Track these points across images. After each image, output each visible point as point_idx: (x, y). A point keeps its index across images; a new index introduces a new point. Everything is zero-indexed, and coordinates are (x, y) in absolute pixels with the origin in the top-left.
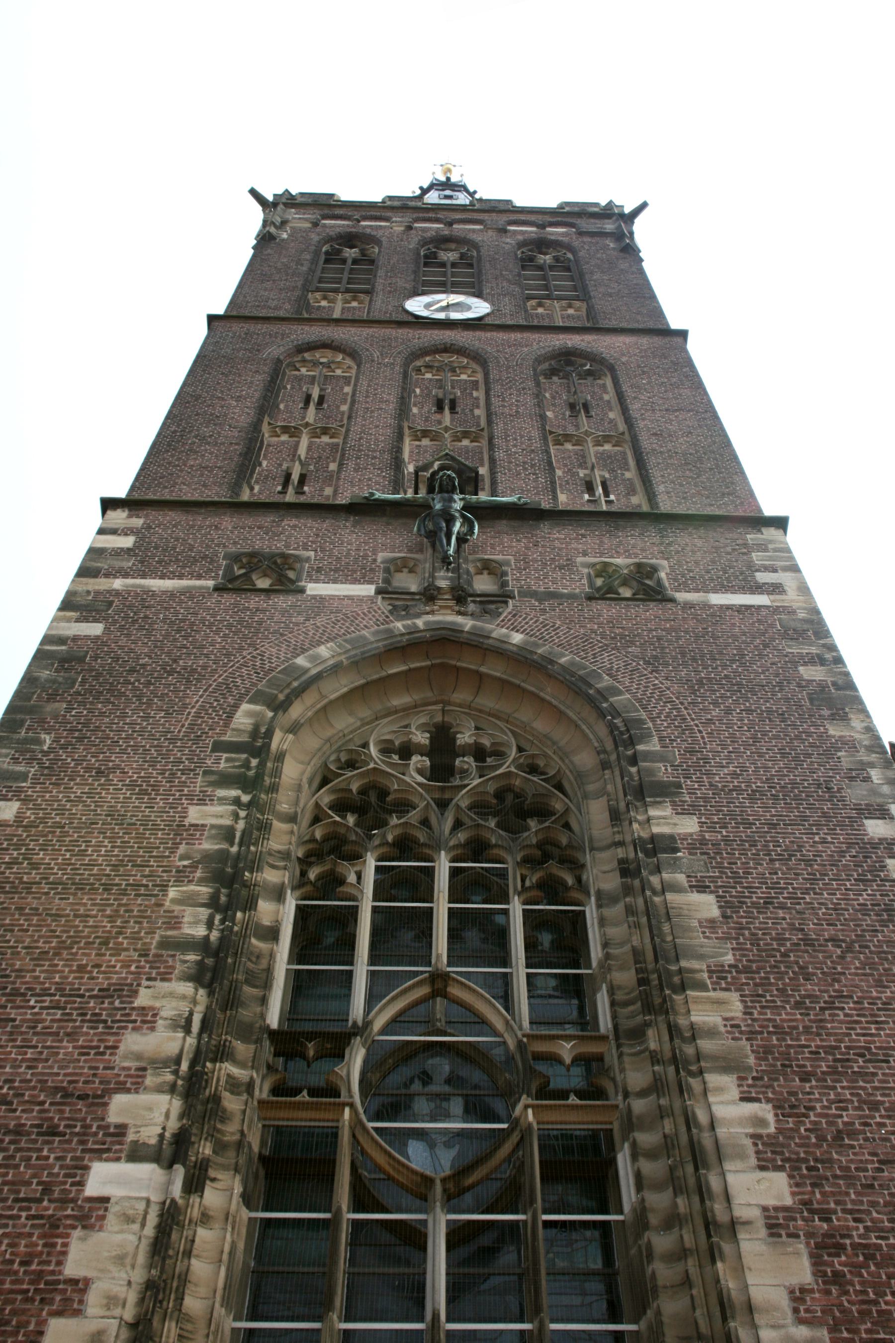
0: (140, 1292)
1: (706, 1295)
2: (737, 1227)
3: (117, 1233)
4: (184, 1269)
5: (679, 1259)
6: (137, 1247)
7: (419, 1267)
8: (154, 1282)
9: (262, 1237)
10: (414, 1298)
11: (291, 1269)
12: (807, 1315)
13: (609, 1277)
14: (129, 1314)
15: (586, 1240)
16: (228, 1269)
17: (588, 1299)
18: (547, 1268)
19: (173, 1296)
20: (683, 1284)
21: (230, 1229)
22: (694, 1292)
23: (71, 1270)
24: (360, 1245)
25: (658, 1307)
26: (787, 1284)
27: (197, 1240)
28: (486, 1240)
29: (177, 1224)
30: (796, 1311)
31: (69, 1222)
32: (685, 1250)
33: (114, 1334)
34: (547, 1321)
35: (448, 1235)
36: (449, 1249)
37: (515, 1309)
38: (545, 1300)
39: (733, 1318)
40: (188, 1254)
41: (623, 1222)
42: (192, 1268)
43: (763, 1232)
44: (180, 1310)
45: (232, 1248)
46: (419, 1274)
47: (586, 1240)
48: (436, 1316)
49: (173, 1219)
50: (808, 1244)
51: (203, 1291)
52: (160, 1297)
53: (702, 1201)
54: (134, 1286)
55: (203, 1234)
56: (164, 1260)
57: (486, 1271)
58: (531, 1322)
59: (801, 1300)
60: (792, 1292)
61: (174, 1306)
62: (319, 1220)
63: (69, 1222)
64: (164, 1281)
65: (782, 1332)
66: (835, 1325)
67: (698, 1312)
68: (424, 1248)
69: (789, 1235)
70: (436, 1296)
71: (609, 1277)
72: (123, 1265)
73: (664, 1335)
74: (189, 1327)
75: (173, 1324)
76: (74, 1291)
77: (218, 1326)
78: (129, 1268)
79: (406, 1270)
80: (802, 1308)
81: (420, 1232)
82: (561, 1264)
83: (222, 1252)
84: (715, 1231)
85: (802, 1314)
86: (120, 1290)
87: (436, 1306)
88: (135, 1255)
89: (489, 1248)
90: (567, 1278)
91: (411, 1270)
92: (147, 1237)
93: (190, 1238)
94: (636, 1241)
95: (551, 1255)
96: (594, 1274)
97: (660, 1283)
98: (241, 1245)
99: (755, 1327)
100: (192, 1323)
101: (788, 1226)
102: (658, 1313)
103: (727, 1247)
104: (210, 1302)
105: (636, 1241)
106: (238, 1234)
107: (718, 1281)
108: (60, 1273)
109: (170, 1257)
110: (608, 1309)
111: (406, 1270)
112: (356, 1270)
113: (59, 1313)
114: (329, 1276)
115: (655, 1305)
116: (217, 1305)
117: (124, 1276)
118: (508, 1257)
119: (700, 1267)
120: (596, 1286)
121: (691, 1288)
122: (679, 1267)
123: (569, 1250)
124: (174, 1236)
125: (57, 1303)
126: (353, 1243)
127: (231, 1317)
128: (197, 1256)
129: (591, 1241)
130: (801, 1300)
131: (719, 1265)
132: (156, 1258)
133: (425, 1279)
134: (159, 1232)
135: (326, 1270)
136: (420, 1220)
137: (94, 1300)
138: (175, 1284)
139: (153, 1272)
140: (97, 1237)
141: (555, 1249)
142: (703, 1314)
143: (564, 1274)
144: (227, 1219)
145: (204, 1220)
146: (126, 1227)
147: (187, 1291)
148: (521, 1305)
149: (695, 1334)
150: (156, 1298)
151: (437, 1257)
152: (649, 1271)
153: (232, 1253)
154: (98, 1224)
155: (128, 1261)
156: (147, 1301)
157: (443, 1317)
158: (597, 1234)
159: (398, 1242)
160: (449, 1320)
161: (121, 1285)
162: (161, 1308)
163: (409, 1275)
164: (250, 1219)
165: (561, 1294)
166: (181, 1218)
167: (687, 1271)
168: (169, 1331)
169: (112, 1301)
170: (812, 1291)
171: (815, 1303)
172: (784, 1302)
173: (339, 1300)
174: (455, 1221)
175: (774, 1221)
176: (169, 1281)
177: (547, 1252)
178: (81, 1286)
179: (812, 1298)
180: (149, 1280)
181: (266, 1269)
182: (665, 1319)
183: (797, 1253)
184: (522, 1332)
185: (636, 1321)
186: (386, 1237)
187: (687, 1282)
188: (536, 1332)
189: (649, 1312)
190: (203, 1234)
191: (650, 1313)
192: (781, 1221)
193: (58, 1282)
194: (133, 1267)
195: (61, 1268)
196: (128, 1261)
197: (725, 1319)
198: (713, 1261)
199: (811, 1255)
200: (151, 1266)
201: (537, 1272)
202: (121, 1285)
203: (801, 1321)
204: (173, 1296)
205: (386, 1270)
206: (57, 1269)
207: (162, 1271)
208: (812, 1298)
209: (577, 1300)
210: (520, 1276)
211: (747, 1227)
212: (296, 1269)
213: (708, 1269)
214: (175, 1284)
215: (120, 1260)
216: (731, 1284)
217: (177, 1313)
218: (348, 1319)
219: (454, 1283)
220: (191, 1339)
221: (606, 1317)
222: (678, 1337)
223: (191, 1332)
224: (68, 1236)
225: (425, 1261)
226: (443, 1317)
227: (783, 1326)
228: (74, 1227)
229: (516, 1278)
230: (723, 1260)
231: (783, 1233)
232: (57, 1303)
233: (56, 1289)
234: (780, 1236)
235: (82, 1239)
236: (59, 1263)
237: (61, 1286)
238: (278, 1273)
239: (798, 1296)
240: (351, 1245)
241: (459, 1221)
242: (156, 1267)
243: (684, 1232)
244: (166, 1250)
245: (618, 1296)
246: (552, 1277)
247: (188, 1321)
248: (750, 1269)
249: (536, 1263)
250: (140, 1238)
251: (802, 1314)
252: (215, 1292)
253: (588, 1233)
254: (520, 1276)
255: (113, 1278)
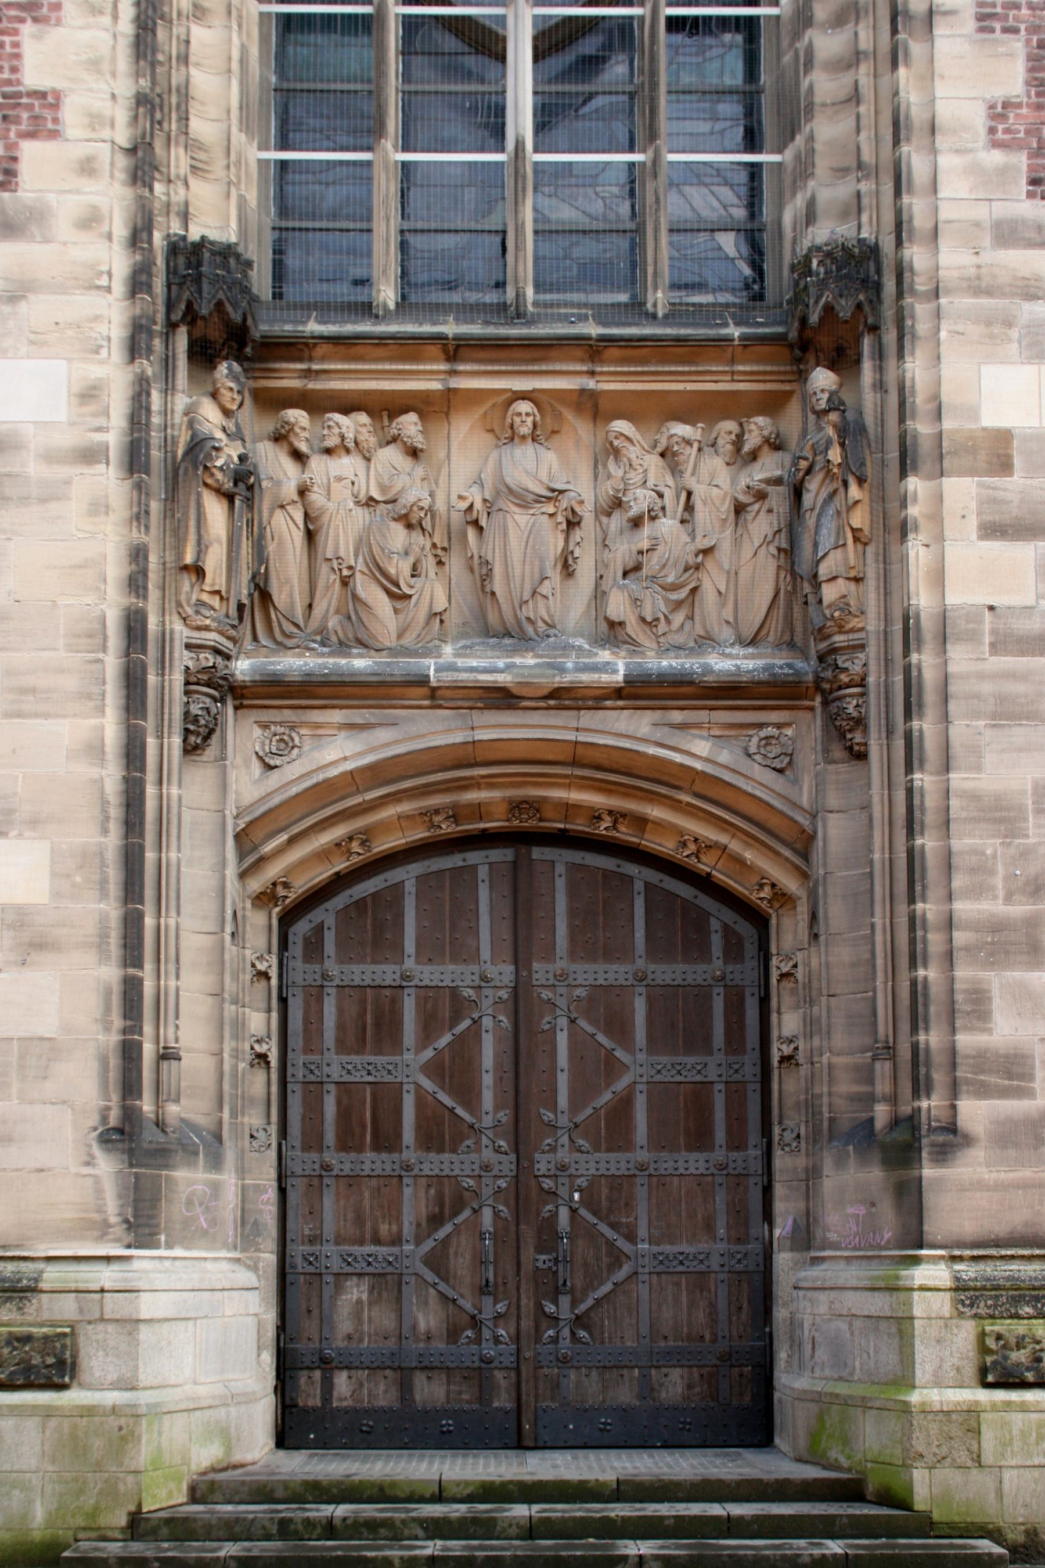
0: (131, 109)
1: (876, 112)
2: (936, 19)
3: (81, 28)
4: (183, 79)
5: (849, 67)
6: (114, 48)
7: (496, 83)
8: (146, 95)
9: (282, 44)
10: (492, 125)
11: (325, 86)
12: (1006, 137)
13: (750, 100)
14: (123, 137)
15: (723, 46)
16: (241, 83)
17: (719, 126)
18: (669, 85)
19: (174, 116)
20: (849, 100)
21: (235, 27)
22: (862, 109)
23: (32, 78)
24: (416, 53)
25: (812, 131)
26: (988, 96)
27: (193, 40)
28: (589, 46)
29: (162, 18)
30: (992, 131)
31: (13, 13)
32: (858, 53)
33: (108, 161)
34: (664, 151)
35: (535, 39)
36: (537, 58)
37: (623, 136)
38: (664, 125)
39: (921, 768)
40: (184, 59)
41: (778, 18)
42: (192, 80)
43: (971, 25)
44: (187, 134)
45: (242, 53)
46: (497, 93)
47: (723, 46)
48: (519, 145)
49: (155, 9)
50: (1028, 42)
51: (213, 112)
52: (158, 116)
53: (898, 193)
54: (119, 100)
55: (199, 33)
56: (153, 64)
57: (587, 88)
58: (644, 151)
59: (1002, 117)
60: (992, 107)
61: (179, 129)
62: (356, 16)
63: (13, 13)
64: (159, 96)
65: (969, 157)
66: (1039, 148)
67: (863, 135)
68: (502, 58)
69: (1005, 30)
70: (520, 119)
71: (750, 100)
72: (99, 72)
73: (813, 166)
74: (202, 156)
75: (181, 151)
76: (43, 106)
77: (239, 155)
78: (108, 77)
79: (480, 88)
80: (1000, 127)
81: (497, 35)
82: (687, 79)
83: (230, 58)
84: (904, 25)
85: (1000, 135)
86: (103, 105)
87: (521, 131)
88: (113, 59)
89: (591, 57)
90: (694, 97)
91: (485, 88)
92: (124, 35)
93: (183, 37)
94: (791, 44)
95: (675, 66)
96: (731, 92)
97: (818, 99)
98: (254, 51)
99: (934, 151)
100: (206, 151)
101: (1006, 17)
102: (811, 138)
103: (916, 48)
104: (225, 126)
105: (791, 44)
106: (248, 35)
107: (896, 93)
108: (19, 82)
109: (161, 63)
110: (745, 138)
111: (480, 88)
112: (412, 88)
113: (31, 135)
114: (376, 95)
115: (808, 128)
116: (234, 130)
117: (105, 87)
118: (617, 69)
119: (875, 76)
120: (731, 108)
121: (858, 103)
122: (846, 79)
123: (700, 59)
124: (161, 34)
125: (25, 122)
126: (407, 51)
127: (255, 145)
128: (197, 65)
129: (731, 47)
130: (1002, 117)
131: (902, 71)
132: (142, 63)
133: (505, 99)
134: (139, 27)
135: (372, 87)
136: (497, 16)
137: (71, 115)
138: (174, 100)
139: (142, 82)
140: (55, 34)
141: (681, 59)
142: (869, 138)
143: (690, 92)
144: (229, 13)
145: (199, 15)
146: (91, 20)
147: (191, 110)
148: (631, 133)
149: (855, 165)
150: (152, 116)
151: (520, 67)
152: (805, 85)
153: (243, 61)
154: (53, 15)
155: (106, 67)
156: (141, 120)
157: (529, 145)
158: (739, 38)
159: (467, 49)
160: (536, 150)
161: (103, 100)
162: (161, 130)
163: (483, 93)
164: (261, 14)
165: (685, 119)
166: (166, 9)
167: (856, 82)
168: (177, 159)
169: (95, 120)
170: (1019, 105)
171: (1019, 122)
172: (980, 121)
173: (393, 122)
174: (545, 18)
175: (988, 10)
176: (165, 96)
177: (670, 63)
178: (49, 100)
179: (1017, 115)
180: (138, 93)
181: (292, 86)
182: (818, 147)
183: (1011, 55)
184: (632, 165)
185: (780, 151)
186: (449, 43)
187: (855, 97)
188: (649, 164)
189: (798, 138)
190: (199, 33)
191: (799, 139)
192: (999, 10)
193: (19, 95)
194: (114, 75)
195: (18, 76)
196: (106, 67)
197: (896, 142)
198: (894, 65)
199: (1030, 58)
200: (138, 74)
201: (654, 86)
202: (103, 100)
203: (996, 144)
204: (174, 116)
205: (453, 88)
206: (13, 77)
207: (154, 82)
208: (1017, 115)
209: (704, 127)
210: (632, 95)
211: (950, 19)
212: (333, 87)
213: (885, 80)
214: (174, 100)
215: (94, 65)
216: (912, 96)
217: (182, 138)
218: (406, 149)
219: (543, 105)
220: (208, 171)
221: (742, 148)
222: (832, 169)
223: (206, 163)
224: (16, 32)
225: (504, 76)
226: (529, 145)
227: (971, 151)
228: (22, 21)
229: (626, 98)
230: (907, 65)
231: (998, 26)
232: (25, 122)
233: (19, 104)
234: (992, 30)
235: (38, 37)
236: (14, 70)
237: (24, 100)
238: (309, 91)
239: (999, 112)
240: (403, 54)
241: (550, 17)
242: (144, 76)
243: (861, 27)
244: (154, 52)
245: (760, 122)
246: (674, 97)
247: (199, 149)
248: (942, 77)
249: (654, 74)
250: (115, 36)
251: (1000, 135)
252: (229, 112)
253: (727, 37)
254: (632, 95)
255: (91, 90)
